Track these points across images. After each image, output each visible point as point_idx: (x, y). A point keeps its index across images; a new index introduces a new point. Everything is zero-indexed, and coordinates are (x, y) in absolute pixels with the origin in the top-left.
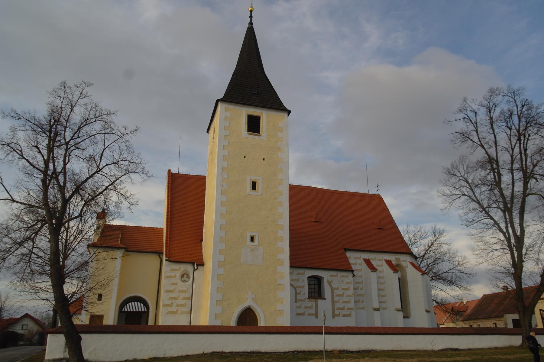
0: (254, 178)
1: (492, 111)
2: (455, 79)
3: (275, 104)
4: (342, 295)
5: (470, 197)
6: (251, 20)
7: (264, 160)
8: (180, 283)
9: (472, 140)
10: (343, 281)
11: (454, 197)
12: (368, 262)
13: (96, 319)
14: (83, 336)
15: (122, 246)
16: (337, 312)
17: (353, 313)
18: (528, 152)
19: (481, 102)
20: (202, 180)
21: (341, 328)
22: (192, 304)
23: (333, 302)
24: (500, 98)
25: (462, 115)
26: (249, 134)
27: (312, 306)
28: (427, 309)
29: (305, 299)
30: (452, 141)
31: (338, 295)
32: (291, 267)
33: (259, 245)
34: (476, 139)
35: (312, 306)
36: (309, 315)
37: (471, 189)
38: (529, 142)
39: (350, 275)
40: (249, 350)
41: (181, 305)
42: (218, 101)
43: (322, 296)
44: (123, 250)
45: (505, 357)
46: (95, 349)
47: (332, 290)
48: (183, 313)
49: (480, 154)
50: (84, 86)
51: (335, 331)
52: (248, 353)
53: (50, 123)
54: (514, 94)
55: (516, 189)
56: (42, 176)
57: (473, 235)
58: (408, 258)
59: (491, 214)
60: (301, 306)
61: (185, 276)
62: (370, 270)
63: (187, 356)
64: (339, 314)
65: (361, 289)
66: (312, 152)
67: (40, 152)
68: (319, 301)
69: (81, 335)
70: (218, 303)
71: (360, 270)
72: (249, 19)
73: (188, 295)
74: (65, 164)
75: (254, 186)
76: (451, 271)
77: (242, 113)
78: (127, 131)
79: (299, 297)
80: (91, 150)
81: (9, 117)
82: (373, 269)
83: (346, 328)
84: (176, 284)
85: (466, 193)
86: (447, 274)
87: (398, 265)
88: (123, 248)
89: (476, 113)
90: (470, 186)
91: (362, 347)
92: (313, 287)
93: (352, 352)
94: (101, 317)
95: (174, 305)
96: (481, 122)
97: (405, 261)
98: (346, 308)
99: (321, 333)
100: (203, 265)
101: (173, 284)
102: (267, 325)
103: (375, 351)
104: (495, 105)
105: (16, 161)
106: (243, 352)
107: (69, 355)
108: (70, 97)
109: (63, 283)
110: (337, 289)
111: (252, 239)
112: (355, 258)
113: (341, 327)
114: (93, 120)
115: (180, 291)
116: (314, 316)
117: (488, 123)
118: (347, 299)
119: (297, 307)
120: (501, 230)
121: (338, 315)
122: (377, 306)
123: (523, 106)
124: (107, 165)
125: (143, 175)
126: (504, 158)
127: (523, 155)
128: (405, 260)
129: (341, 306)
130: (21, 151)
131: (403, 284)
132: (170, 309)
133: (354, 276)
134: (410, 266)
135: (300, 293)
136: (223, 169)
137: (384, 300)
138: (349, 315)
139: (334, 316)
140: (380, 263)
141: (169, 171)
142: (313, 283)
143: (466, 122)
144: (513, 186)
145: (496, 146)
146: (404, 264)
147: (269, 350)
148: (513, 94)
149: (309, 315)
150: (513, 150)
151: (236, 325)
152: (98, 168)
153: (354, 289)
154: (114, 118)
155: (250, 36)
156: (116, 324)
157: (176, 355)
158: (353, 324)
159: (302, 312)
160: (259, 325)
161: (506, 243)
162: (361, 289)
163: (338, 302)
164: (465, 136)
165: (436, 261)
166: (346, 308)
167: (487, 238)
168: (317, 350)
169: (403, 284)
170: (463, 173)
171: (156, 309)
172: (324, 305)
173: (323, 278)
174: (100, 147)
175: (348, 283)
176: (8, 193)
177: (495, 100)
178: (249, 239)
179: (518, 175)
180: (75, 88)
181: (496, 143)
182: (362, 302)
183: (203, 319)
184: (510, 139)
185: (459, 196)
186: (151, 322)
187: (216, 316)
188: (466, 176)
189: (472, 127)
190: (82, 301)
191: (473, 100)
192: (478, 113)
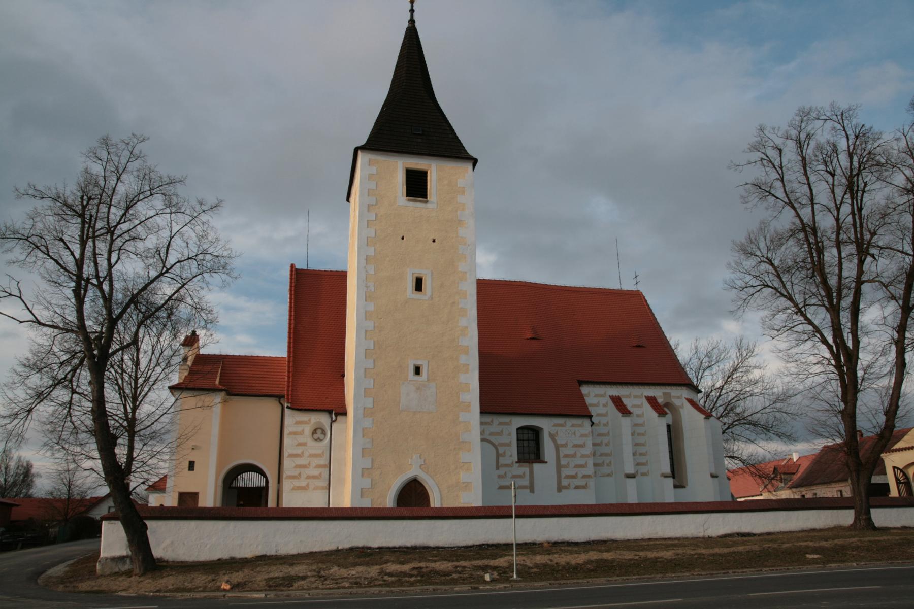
0: (419, 272)
1: (805, 147)
2: (720, 104)
3: (450, 147)
4: (574, 456)
5: (775, 288)
6: (412, 16)
7: (434, 241)
8: (311, 443)
9: (774, 196)
11: (752, 290)
12: (618, 402)
14: (149, 523)
15: (221, 387)
16: (565, 482)
17: (592, 483)
18: (863, 212)
19: (787, 132)
20: (341, 277)
23: (559, 467)
24: (819, 123)
25: (757, 156)
28: (713, 472)
30: (742, 197)
31: (566, 456)
32: (483, 412)
34: (780, 194)
37: (779, 276)
38: (865, 195)
39: (587, 422)
40: (409, 545)
41: (314, 477)
42: (356, 150)
43: (539, 458)
44: (223, 394)
45: (817, 545)
46: (172, 543)
47: (557, 447)
49: (786, 220)
50: (135, 141)
52: (407, 548)
53: (82, 202)
54: (842, 117)
55: (845, 274)
56: (73, 284)
57: (781, 351)
58: (685, 393)
59: (809, 315)
61: (319, 432)
62: (620, 414)
63: (311, 553)
64: (569, 485)
65: (606, 445)
66: (502, 229)
67: (68, 248)
68: (536, 466)
70: (364, 472)
71: (605, 415)
72: (409, 14)
73: (324, 461)
74: (110, 266)
75: (419, 285)
76: (767, 410)
77: (396, 168)
78: (204, 208)
79: (502, 461)
80: (151, 242)
81: (25, 197)
82: (624, 410)
83: (568, 506)
84: (304, 444)
85: (770, 284)
86: (759, 415)
87: (667, 405)
88: (221, 390)
89: (780, 150)
90: (777, 271)
91: (593, 536)
92: (526, 444)
93: (577, 544)
94: (194, 496)
95: (304, 476)
96: (789, 166)
97: (678, 398)
98: (580, 475)
100: (344, 413)
101: (300, 444)
102: (445, 506)
103: (614, 541)
104: (809, 136)
105: (39, 263)
106: (400, 547)
108: (116, 159)
109: (115, 444)
110: (565, 445)
111: (417, 371)
112: (596, 396)
113: (560, 506)
114: (149, 193)
115: (311, 456)
116: (528, 490)
117: (798, 167)
118: (582, 462)
119: (499, 477)
120: (824, 341)
121: (566, 488)
122: (630, 470)
123: (857, 137)
125: (224, 276)
126: (826, 222)
127: (857, 217)
128: (679, 395)
129: (571, 472)
130: (47, 248)
131: (674, 435)
132: (297, 483)
133: (593, 424)
134: (688, 406)
135: (504, 455)
137: (644, 461)
138: (585, 487)
140: (637, 402)
141: (292, 266)
143: (764, 166)
144: (841, 269)
145: (813, 204)
146: (677, 402)
147: (441, 544)
148: (840, 117)
150: (838, 209)
151: (395, 506)
152: (164, 266)
153: (594, 444)
154: (180, 189)
155: (412, 41)
157: (294, 551)
158: (592, 501)
160: (432, 505)
161: (833, 362)
162: (606, 445)
163: (567, 466)
164: (763, 190)
165: (740, 396)
166: (580, 475)
167: (804, 356)
169: (674, 435)
170: (764, 251)
171: (279, 482)
173: (542, 429)
174: (166, 234)
175: (582, 436)
176: (31, 312)
177: (809, 128)
178: (411, 370)
179: (849, 249)
180: (124, 146)
181: (812, 200)
182: (609, 465)
183: (344, 499)
184: (833, 192)
185: (758, 288)
186: (271, 503)
188: (769, 255)
189: (774, 175)
191: (774, 129)
192: (785, 150)
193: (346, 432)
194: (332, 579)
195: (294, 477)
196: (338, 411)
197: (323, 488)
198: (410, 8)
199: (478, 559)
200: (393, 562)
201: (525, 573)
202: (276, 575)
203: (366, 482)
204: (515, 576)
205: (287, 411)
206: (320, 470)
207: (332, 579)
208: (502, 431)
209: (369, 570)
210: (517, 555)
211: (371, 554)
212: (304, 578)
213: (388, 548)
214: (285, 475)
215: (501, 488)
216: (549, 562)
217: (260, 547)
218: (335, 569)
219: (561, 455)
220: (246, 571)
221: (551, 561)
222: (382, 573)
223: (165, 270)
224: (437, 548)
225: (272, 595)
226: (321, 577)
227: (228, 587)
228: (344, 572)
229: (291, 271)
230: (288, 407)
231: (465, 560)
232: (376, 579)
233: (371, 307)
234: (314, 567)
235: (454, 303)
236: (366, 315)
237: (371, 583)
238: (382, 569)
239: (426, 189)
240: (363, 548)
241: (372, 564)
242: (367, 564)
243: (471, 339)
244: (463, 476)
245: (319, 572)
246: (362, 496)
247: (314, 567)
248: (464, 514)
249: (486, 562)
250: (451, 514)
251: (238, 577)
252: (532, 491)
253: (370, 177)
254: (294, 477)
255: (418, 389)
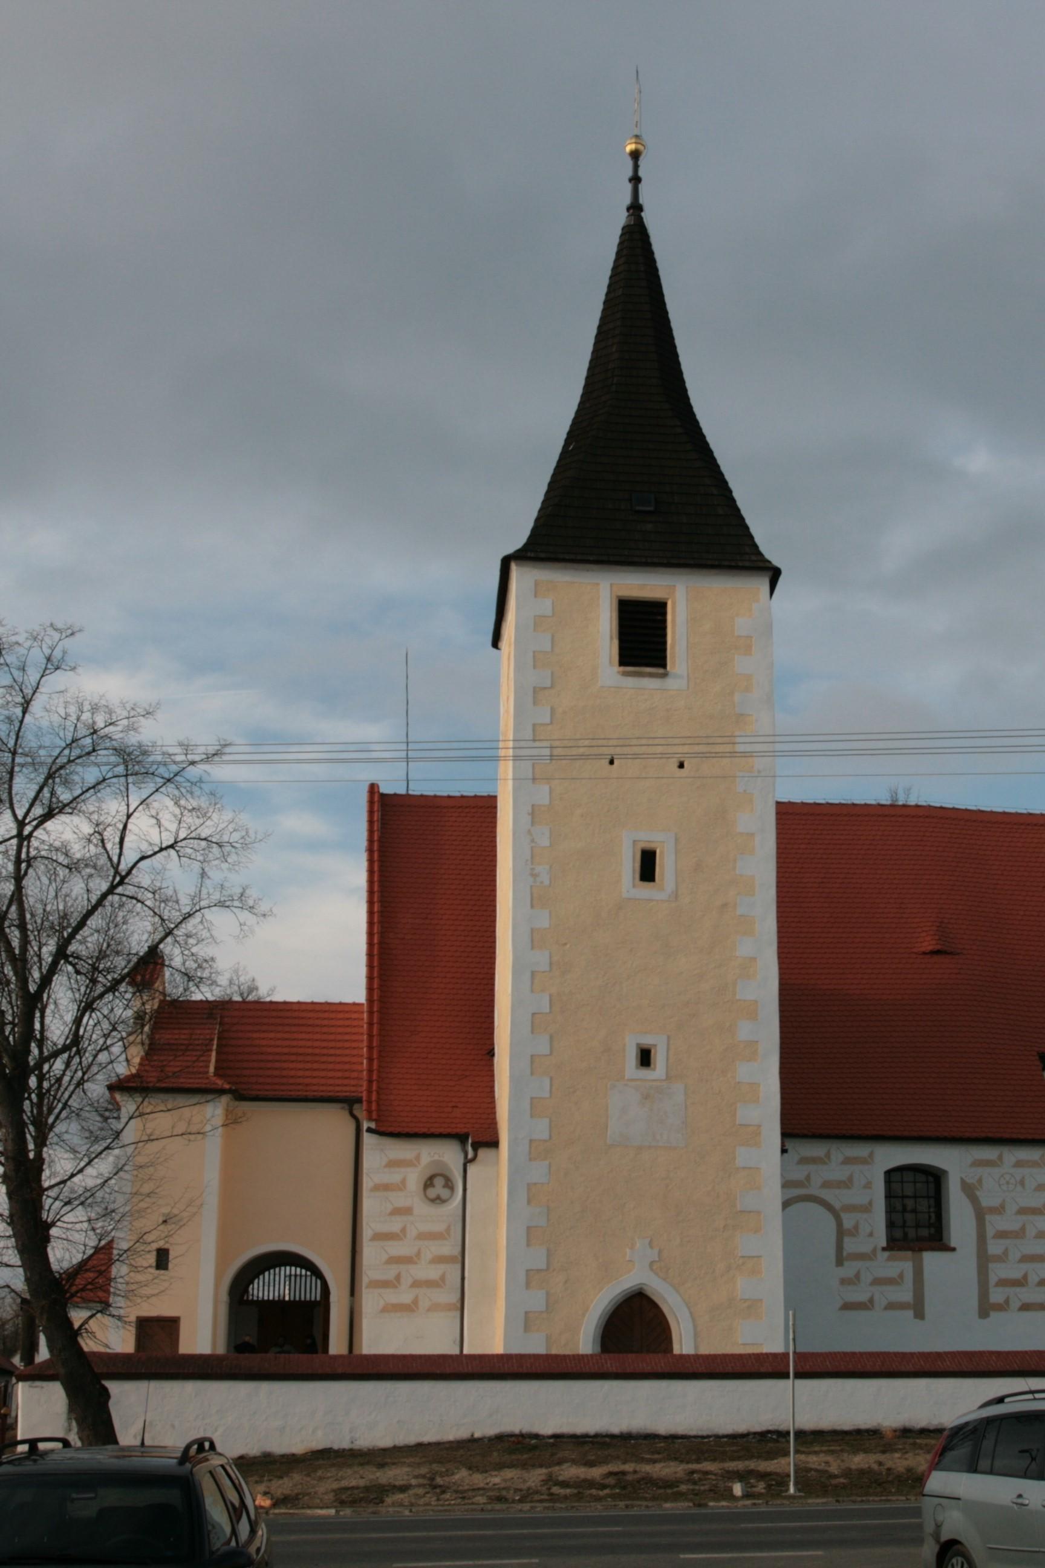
0: (649, 838)
3: (721, 542)
4: (1019, 1234)
8: (422, 1208)
10: (1022, 1183)
13: (158, 1332)
14: (114, 1387)
15: (220, 1083)
16: (997, 1295)
20: (483, 809)
21: (939, 1355)
22: (463, 1279)
23: (984, 1260)
26: (626, 674)
27: (901, 1276)
29: (874, 1251)
31: (1002, 1235)
33: (668, 1077)
35: (901, 1276)
36: (891, 1306)
40: (615, 1430)
41: (430, 1284)
43: (941, 1239)
44: (225, 1099)
47: (980, 1215)
48: (434, 1308)
51: (910, 1368)
52: (612, 1436)
60: (857, 1276)
61: (439, 1182)
63: (420, 1445)
68: (931, 1259)
69: (108, 1384)
72: (629, 187)
73: (449, 1248)
77: (596, 596)
79: (851, 1245)
84: (407, 1211)
88: (221, 1092)
91: (617, 1425)
94: (169, 1326)
95: (406, 1282)
99: (786, 1376)
100: (494, 1144)
101: (397, 1212)
106: (596, 1436)
107: (80, 1438)
109: (47, 1239)
110: (999, 1210)
111: (645, 1058)
115: (423, 1236)
116: (910, 1313)
119: (844, 1281)
124: (143, 858)
125: (244, 916)
132: (392, 1297)
135: (854, 1232)
136: (535, 813)
139: (985, 1309)
141: (373, 788)
142: (909, 1190)
147: (680, 1430)
149: (891, 1306)
151: (598, 1349)
152: (117, 872)
155: (636, 257)
156: (221, 1350)
157: (386, 1442)
159: (862, 1297)
160: (677, 1350)
163: (1002, 1258)
166: (1033, 1279)
168: (846, 1428)
172: (948, 1273)
173: (945, 1172)
178: (632, 1057)
183: (491, 1338)
186: (337, 1345)
187: (529, 1322)
190: (112, 1248)
193: (494, 1180)
194: (456, 1492)
195: (385, 1284)
196: (480, 1137)
197: (449, 1307)
198: (630, 173)
199: (739, 1458)
200: (574, 1462)
201: (810, 1482)
202: (354, 1483)
203: (536, 1300)
204: (792, 1490)
205: (368, 1139)
206: (442, 1268)
207: (456, 1492)
208: (850, 1179)
209: (526, 1475)
210: (797, 1452)
211: (535, 1447)
212: (403, 1489)
213: (574, 1437)
214: (365, 1280)
215: (847, 1306)
216: (875, 1467)
217: (320, 1433)
218: (463, 1473)
219: (990, 1232)
220: (297, 1477)
221: (880, 1464)
222: (550, 1480)
223: (118, 879)
224: (673, 1437)
225: (347, 1512)
226: (435, 1487)
227: (267, 1503)
228: (478, 1479)
229: (371, 802)
230: (369, 1130)
231: (714, 1460)
232: (537, 1492)
233: (543, 921)
234: (423, 1470)
235: (725, 905)
236: (535, 939)
237: (527, 1496)
238: (550, 1475)
239: (665, 643)
240: (522, 1435)
241: (534, 1466)
242: (524, 1466)
243: (764, 986)
244: (743, 1287)
245: (432, 1479)
246: (527, 1328)
247: (423, 1470)
248: (729, 1369)
249: (752, 1464)
250: (702, 1369)
251: (284, 1486)
252: (920, 1314)
253: (539, 622)
254: (385, 1284)
255: (647, 1097)
